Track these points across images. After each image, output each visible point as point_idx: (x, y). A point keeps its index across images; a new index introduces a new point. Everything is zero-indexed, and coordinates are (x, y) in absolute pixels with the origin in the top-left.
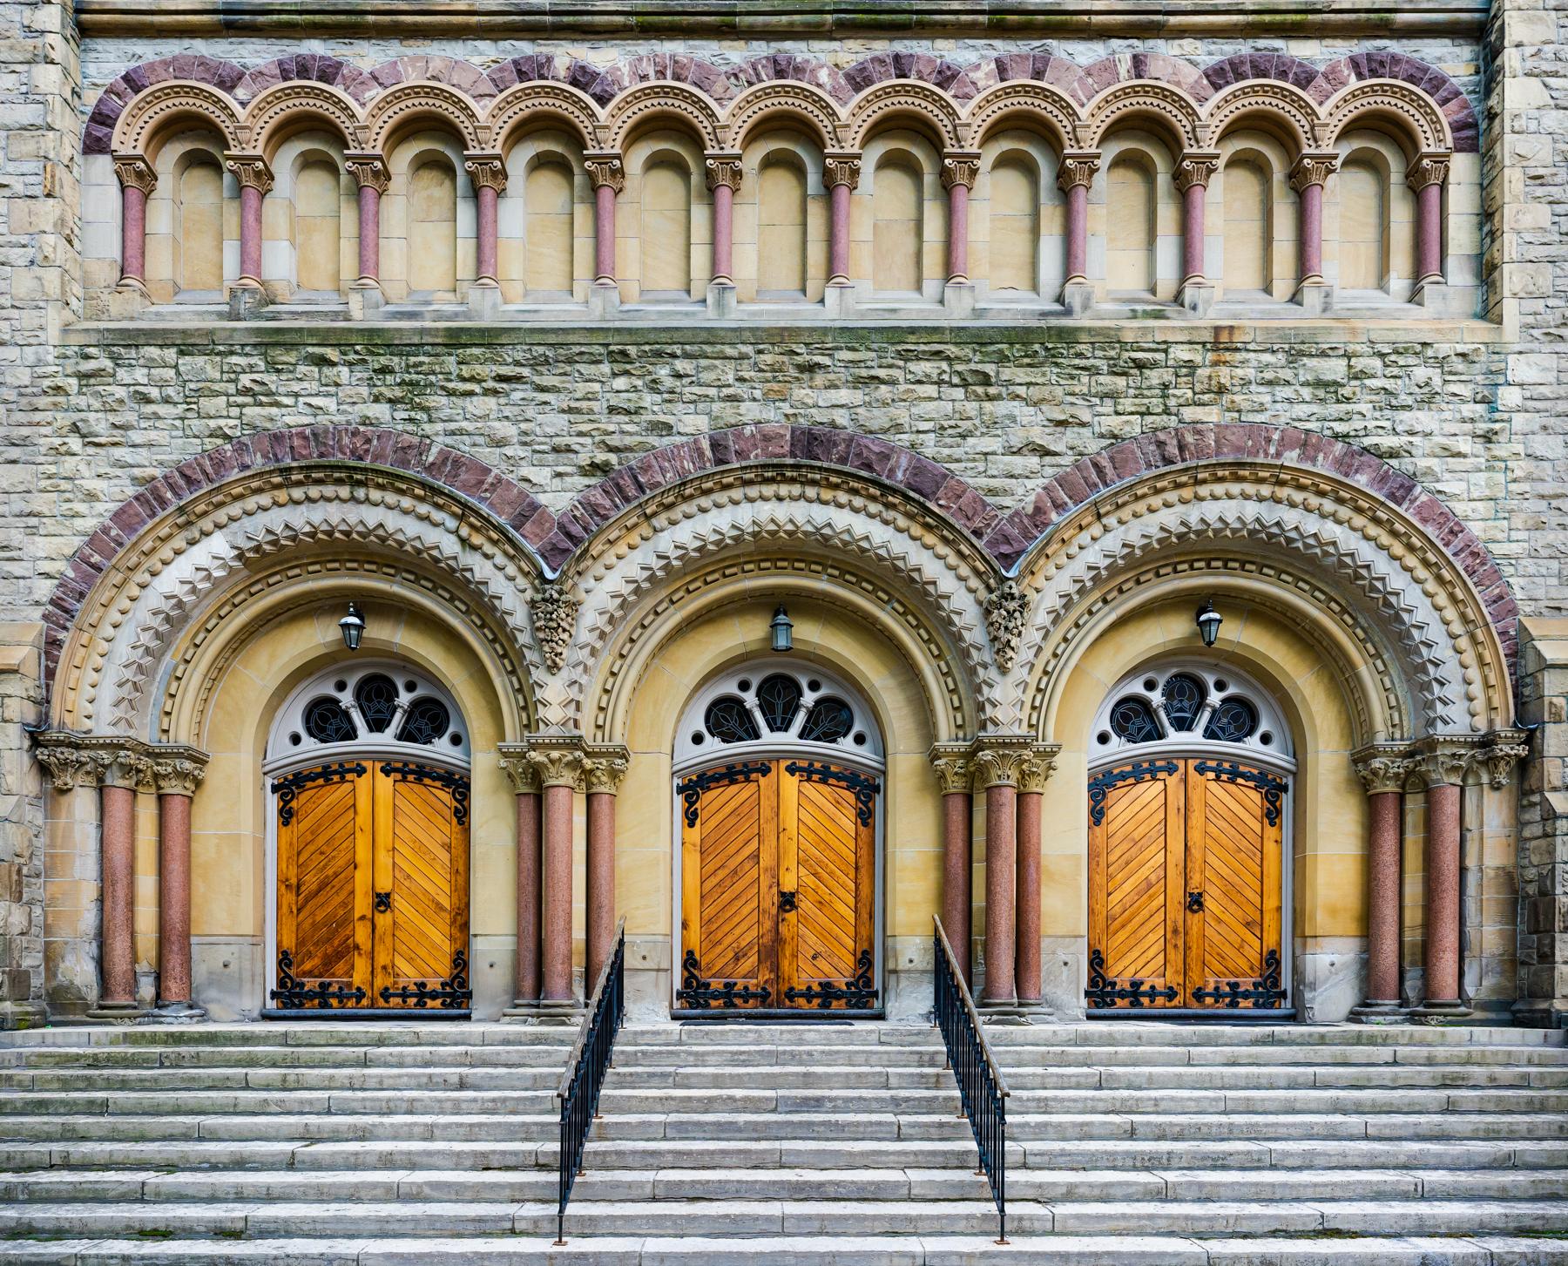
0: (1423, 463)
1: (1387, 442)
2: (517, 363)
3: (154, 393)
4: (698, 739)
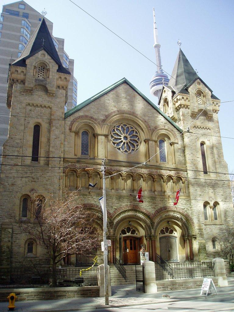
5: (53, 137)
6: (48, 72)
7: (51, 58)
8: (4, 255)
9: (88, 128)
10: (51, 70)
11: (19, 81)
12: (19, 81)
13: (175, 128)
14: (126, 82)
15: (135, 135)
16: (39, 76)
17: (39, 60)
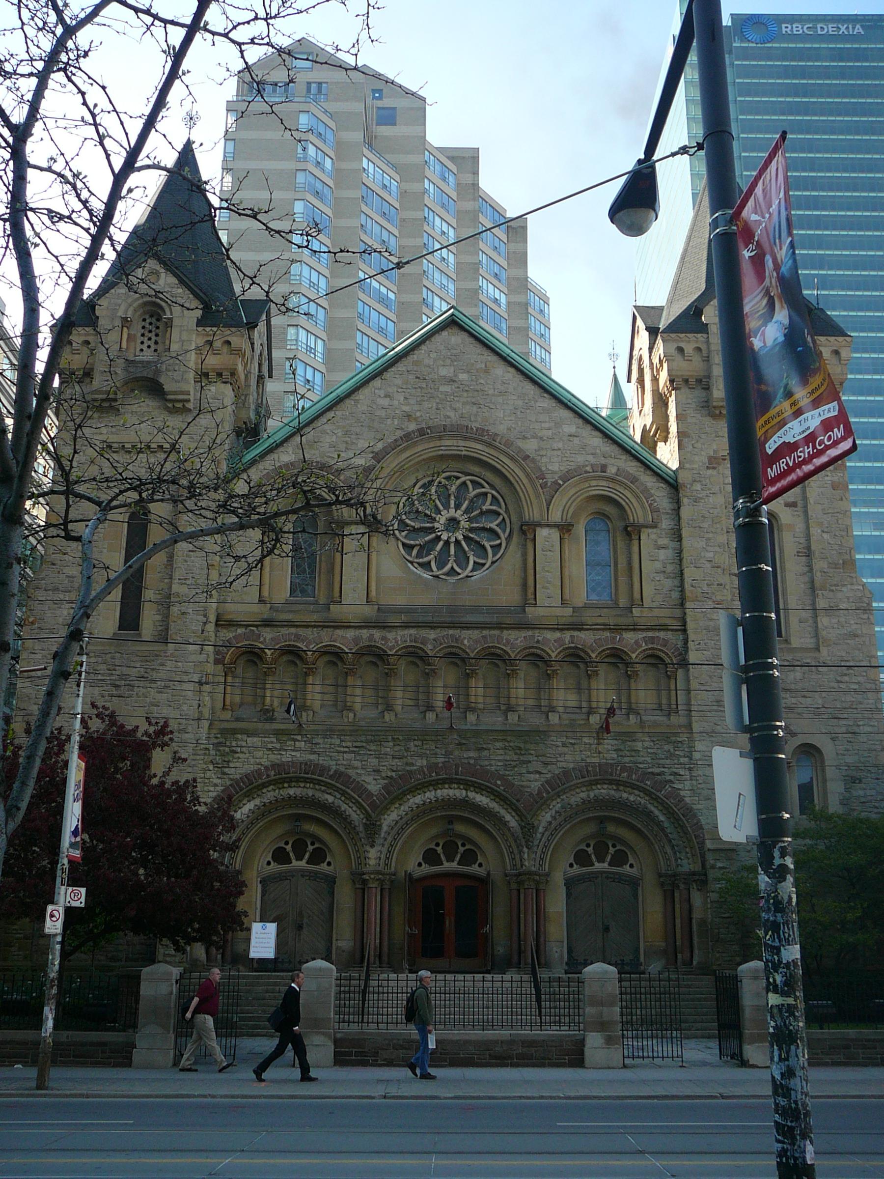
0: (668, 778)
1: (657, 770)
2: (362, 741)
3: (239, 750)
4: (269, 863)
7: (177, 282)
8: (15, 927)
10: (175, 322)
13: (649, 472)
15: (490, 512)
16: (144, 347)
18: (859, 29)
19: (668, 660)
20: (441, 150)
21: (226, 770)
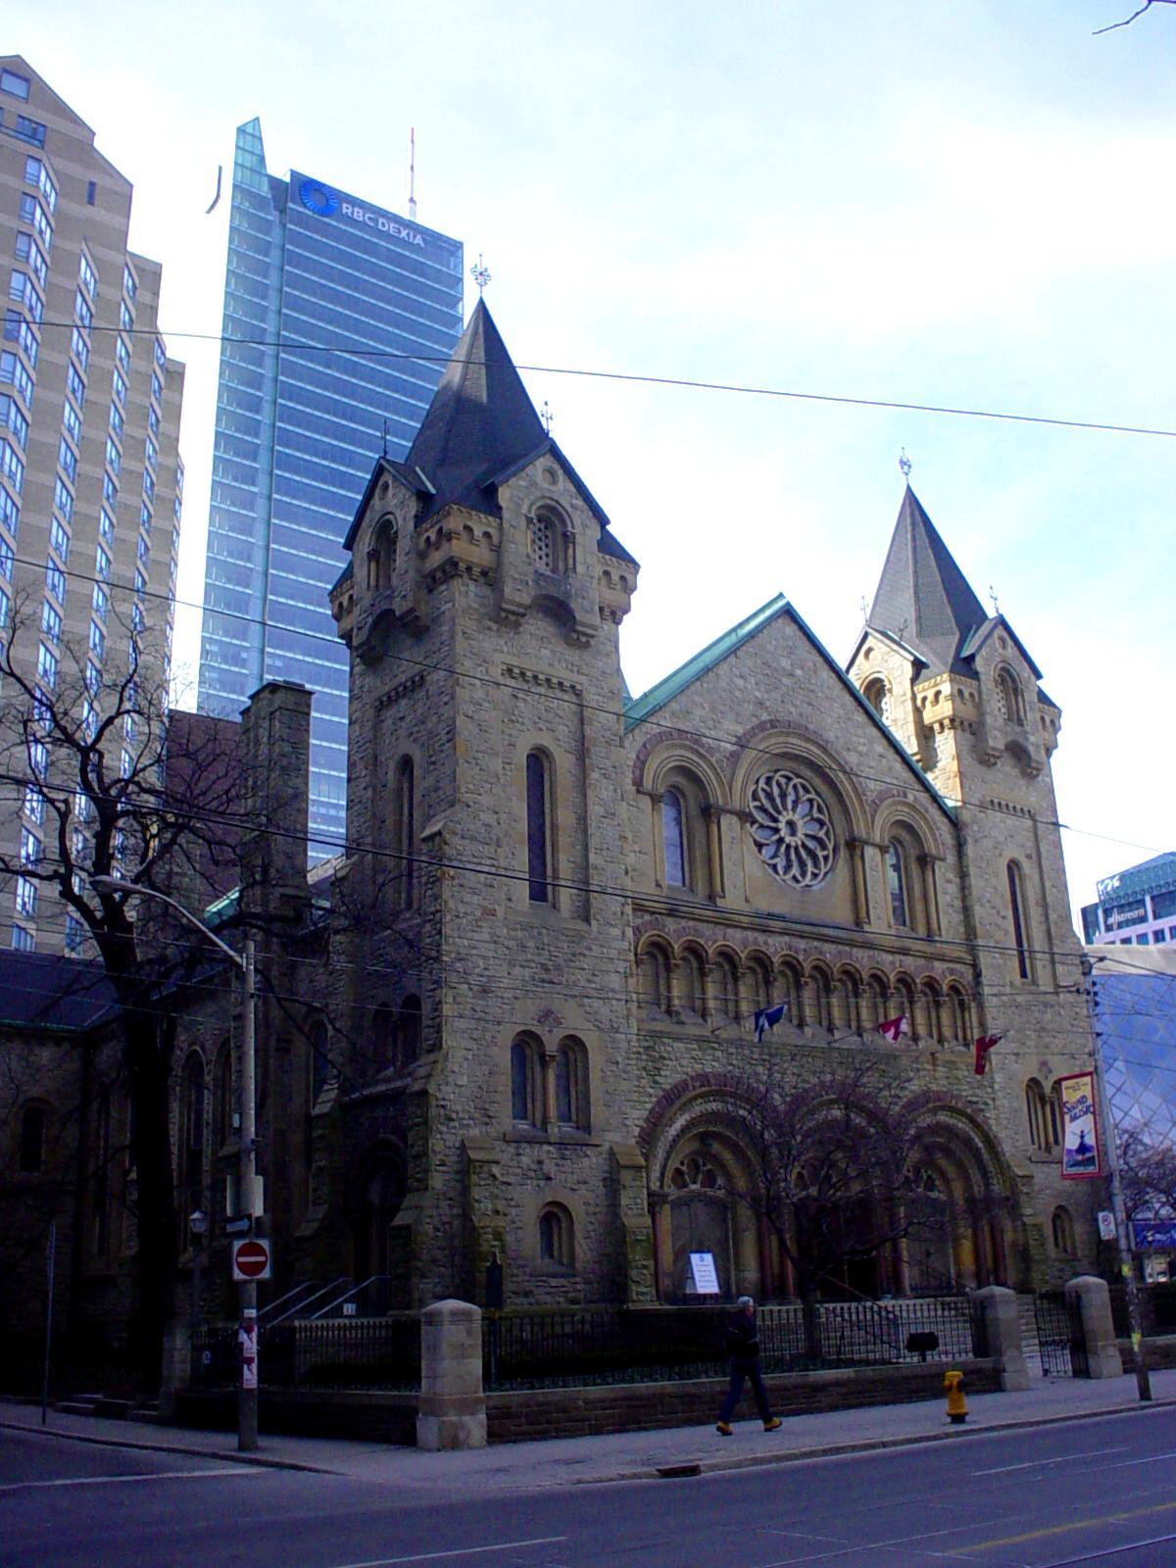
5: (595, 810)
6: (571, 545)
9: (681, 781)
11: (476, 571)
12: (476, 571)
14: (789, 613)
17: (539, 494)
18: (418, 240)
19: (963, 991)
20: (132, 255)
21: (658, 1078)
